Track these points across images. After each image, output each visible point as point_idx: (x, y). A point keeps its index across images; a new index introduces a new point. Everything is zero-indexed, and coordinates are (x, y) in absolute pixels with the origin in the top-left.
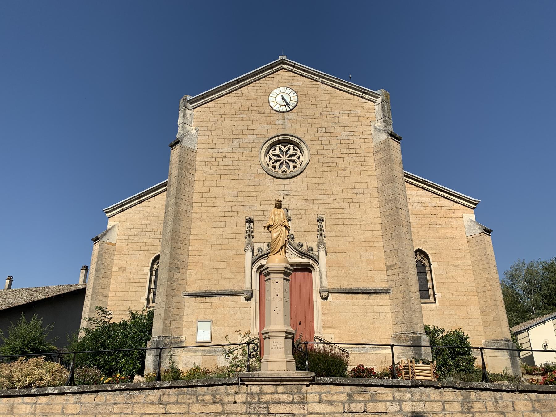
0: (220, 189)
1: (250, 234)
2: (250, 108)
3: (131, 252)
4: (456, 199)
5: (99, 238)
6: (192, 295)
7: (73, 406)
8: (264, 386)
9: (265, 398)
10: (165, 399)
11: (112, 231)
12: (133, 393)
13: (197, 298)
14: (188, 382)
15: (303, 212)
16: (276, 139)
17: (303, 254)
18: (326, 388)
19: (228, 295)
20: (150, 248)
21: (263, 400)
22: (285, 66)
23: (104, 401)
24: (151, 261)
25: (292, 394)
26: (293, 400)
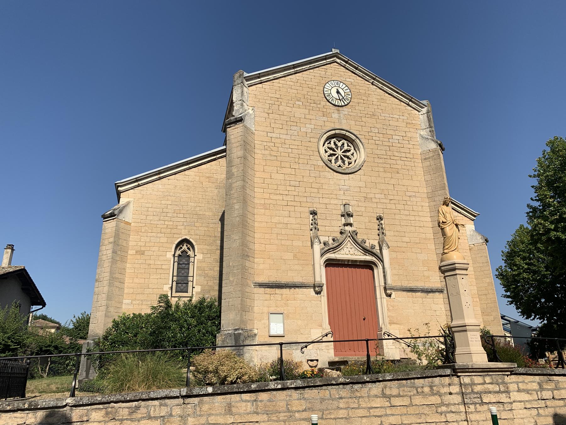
0: (281, 177)
1: (315, 226)
2: (306, 96)
3: (149, 234)
4: (460, 210)
5: (115, 215)
6: (261, 285)
7: (297, 402)
8: (473, 377)
9: (478, 388)
10: (388, 392)
11: (127, 208)
12: (356, 387)
13: (266, 289)
14: (408, 375)
15: (363, 209)
16: (333, 132)
17: (366, 251)
18: (521, 378)
19: (298, 287)
20: (173, 231)
21: (475, 391)
22: (338, 61)
23: (329, 396)
24: (174, 246)
25: (498, 384)
26: (500, 390)
